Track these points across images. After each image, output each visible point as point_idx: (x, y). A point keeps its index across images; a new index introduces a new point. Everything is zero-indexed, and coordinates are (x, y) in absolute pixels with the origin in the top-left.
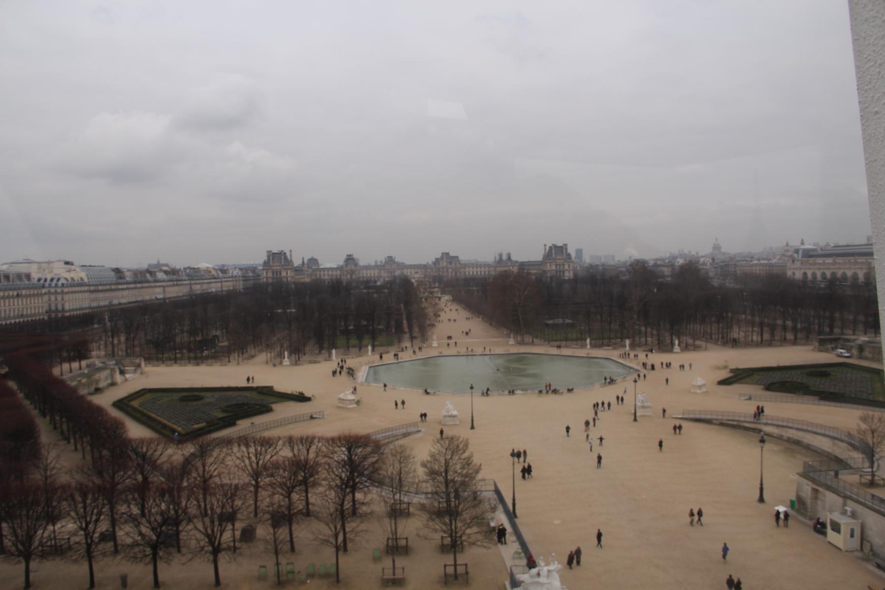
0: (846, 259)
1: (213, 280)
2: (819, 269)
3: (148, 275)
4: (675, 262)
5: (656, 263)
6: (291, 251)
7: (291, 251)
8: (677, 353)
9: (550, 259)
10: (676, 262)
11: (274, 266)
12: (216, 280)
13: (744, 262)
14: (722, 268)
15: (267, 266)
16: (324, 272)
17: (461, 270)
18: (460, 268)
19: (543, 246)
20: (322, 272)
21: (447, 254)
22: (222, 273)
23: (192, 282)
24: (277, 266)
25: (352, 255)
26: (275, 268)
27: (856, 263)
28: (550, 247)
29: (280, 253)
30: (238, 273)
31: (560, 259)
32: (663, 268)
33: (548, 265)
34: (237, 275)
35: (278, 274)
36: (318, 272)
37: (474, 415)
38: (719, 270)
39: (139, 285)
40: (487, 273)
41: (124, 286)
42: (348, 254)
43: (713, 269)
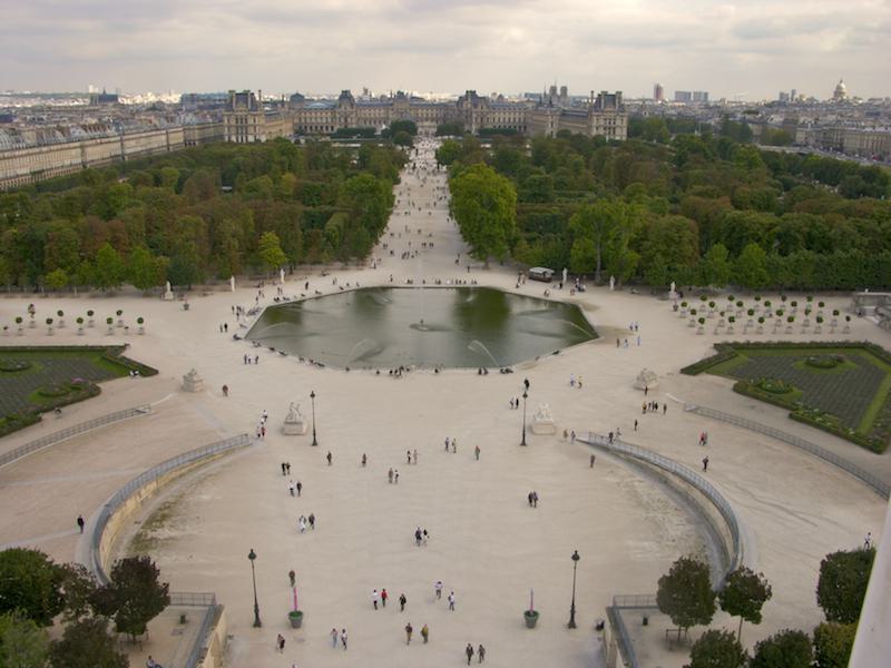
1: (154, 133)
3: (58, 133)
23: (124, 137)
33: (595, 118)
37: (258, 602)
38: (822, 135)
39: (45, 149)
41: (24, 152)
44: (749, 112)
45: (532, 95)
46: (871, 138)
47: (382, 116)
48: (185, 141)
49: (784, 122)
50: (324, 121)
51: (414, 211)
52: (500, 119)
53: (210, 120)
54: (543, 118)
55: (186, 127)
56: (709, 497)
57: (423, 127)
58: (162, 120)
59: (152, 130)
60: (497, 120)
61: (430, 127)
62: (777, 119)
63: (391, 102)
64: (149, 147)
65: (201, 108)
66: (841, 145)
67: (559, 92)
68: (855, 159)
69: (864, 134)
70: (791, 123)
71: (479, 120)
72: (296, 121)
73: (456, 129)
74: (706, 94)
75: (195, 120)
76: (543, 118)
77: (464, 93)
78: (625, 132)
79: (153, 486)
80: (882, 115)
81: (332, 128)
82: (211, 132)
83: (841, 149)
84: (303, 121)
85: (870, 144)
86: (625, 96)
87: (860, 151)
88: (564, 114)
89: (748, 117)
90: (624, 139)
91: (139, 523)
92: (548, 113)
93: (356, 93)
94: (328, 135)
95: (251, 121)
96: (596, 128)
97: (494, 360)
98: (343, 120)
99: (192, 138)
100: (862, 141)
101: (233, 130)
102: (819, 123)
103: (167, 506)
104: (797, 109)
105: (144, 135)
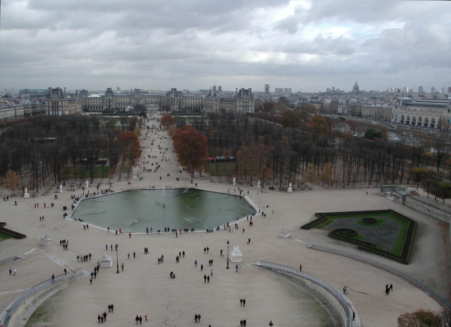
0: (429, 109)
1: (8, 109)
2: (412, 114)
4: (323, 101)
5: (312, 101)
6: (65, 88)
7: (65, 88)
8: (290, 192)
9: (239, 98)
10: (324, 101)
11: (53, 98)
12: (11, 109)
13: (366, 105)
14: (352, 108)
15: (48, 98)
16: (91, 100)
17: (183, 101)
18: (183, 100)
19: (236, 89)
20: (90, 100)
21: (175, 89)
22: (16, 103)
24: (55, 98)
25: (111, 88)
26: (54, 99)
27: (435, 112)
28: (240, 90)
29: (58, 90)
30: (28, 102)
31: (246, 99)
32: (315, 104)
33: (238, 102)
34: (28, 104)
35: (56, 104)
36: (87, 100)
38: (350, 109)
40: (200, 103)
42: (108, 88)
43: (347, 108)
44: (314, 98)
45: (203, 91)
46: (374, 110)
47: (128, 101)
48: (25, 114)
49: (331, 103)
50: (98, 104)
51: (161, 155)
52: (190, 102)
53: (38, 103)
54: (211, 102)
55: (25, 106)
56: (328, 290)
57: (150, 107)
58: (13, 102)
59: (7, 108)
60: (187, 103)
61: (154, 107)
62: (328, 101)
63: (132, 94)
64: (6, 116)
65: (31, 96)
66: (360, 113)
67: (217, 89)
68: (368, 121)
69: (372, 108)
70: (335, 103)
71: (178, 103)
72: (83, 104)
73: (167, 108)
74: (290, 89)
75: (30, 102)
76: (211, 102)
77: (170, 90)
78: (253, 109)
79: (32, 299)
80: (377, 98)
81: (102, 107)
82: (38, 109)
83: (360, 116)
84: (87, 104)
85: (374, 112)
86: (252, 91)
87: (370, 116)
88: (222, 100)
89: (314, 100)
90: (253, 112)
91: (26, 319)
92: (214, 99)
93: (114, 89)
94: (100, 111)
95: (60, 104)
96: (239, 108)
97: (202, 222)
98: (108, 104)
99: (28, 112)
100: (370, 111)
101: (51, 109)
102: (349, 103)
103: (39, 309)
104: (336, 96)
105: (3, 110)
